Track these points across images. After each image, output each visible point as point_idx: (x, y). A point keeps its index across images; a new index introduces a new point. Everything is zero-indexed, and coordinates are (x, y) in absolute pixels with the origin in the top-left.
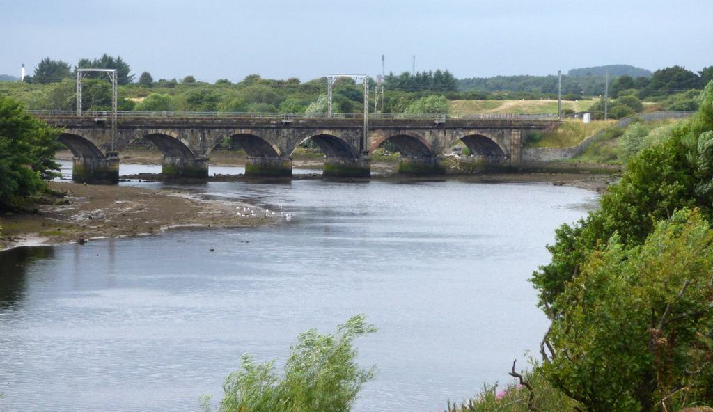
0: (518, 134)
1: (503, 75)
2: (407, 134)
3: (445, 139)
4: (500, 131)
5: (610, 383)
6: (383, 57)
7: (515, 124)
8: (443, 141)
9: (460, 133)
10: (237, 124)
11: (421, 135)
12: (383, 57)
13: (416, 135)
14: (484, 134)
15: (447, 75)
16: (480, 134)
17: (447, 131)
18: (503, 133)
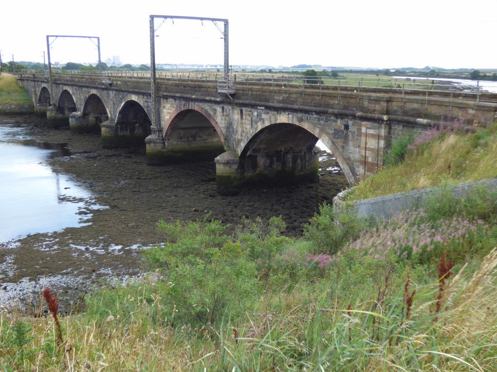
0: (379, 137)
1: (69, 227)
2: (196, 109)
3: (242, 124)
4: (339, 121)
5: (176, 176)
6: (66, 188)
7: (372, 106)
8: (240, 129)
9: (264, 116)
10: (86, 83)
11: (212, 113)
12: (66, 188)
13: (206, 111)
14: (306, 126)
15: (67, 228)
16: (297, 123)
17: (244, 109)
18: (347, 127)
